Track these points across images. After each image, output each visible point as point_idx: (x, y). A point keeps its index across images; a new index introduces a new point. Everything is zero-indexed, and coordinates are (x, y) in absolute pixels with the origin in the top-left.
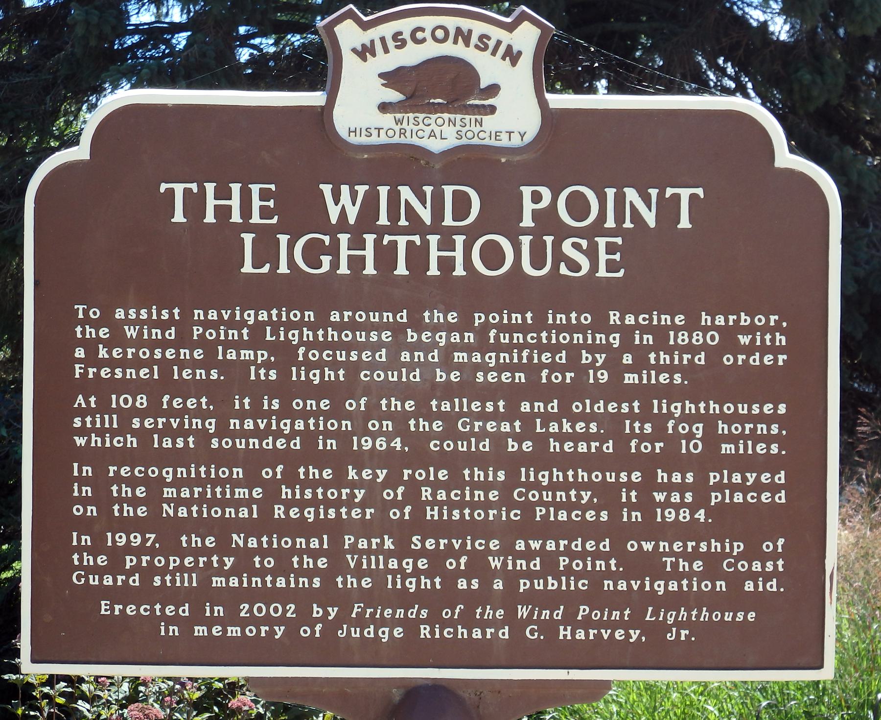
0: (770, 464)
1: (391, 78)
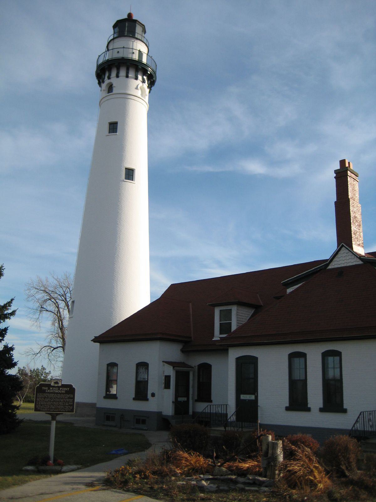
0: (72, 402)
1: (54, 382)
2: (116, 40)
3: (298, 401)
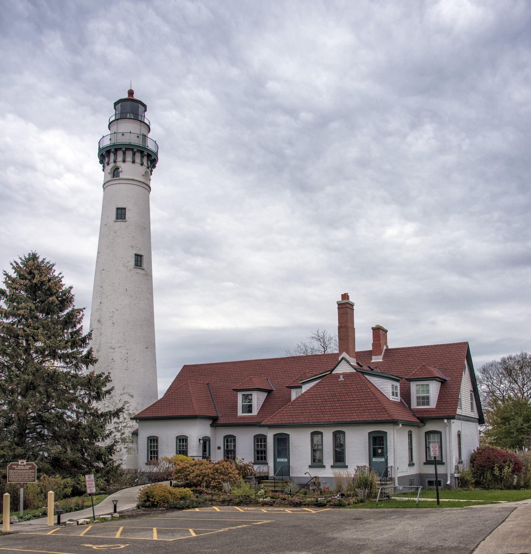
2: (119, 121)
3: (317, 462)
